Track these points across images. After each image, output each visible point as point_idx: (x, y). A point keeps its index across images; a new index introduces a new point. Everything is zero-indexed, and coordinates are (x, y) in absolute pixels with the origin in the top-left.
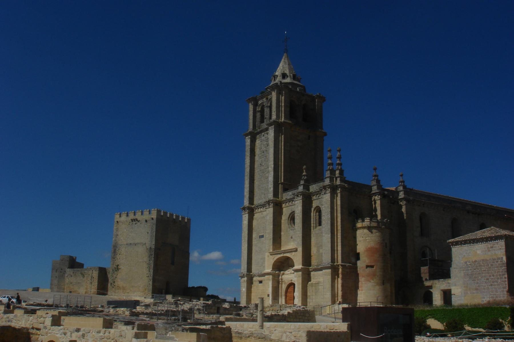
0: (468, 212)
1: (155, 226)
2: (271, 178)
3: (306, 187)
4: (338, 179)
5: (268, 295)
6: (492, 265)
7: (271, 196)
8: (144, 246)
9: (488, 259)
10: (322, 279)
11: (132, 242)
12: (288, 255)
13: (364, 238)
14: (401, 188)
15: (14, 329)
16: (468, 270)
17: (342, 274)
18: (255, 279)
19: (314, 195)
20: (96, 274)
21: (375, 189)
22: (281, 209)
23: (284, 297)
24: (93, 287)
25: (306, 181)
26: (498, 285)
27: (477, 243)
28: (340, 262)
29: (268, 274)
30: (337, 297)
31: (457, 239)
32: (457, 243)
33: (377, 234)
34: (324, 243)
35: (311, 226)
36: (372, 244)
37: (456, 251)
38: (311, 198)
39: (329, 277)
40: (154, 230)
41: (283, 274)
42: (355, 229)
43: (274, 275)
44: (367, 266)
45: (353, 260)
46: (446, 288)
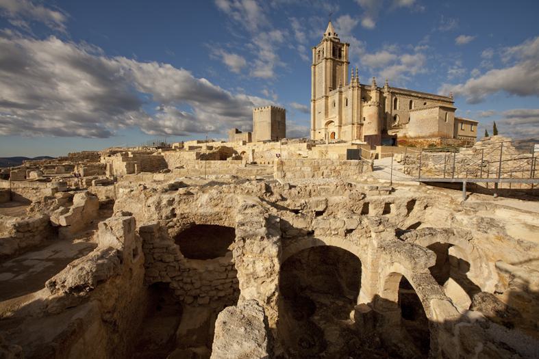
2: (324, 86)
7: (324, 94)
15: (228, 148)
34: (348, 113)
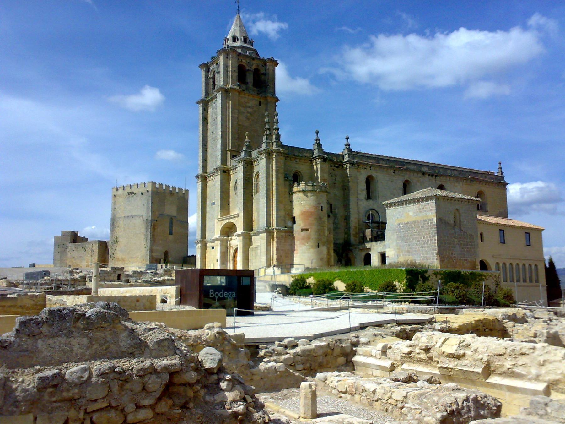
0: (424, 174)
1: (150, 199)
2: (219, 146)
3: (249, 153)
4: (275, 144)
5: (217, 261)
6: (423, 227)
7: (219, 164)
8: (141, 218)
9: (419, 220)
10: (259, 241)
11: (130, 215)
12: (231, 220)
13: (300, 202)
14: (346, 151)
16: (401, 232)
17: (277, 238)
18: (208, 245)
19: (255, 161)
20: (96, 248)
21: (316, 153)
22: (229, 175)
23: (232, 262)
24: (93, 260)
25: (248, 147)
26: (428, 247)
27: (410, 203)
28: (275, 226)
29: (217, 240)
30: (273, 260)
31: (391, 201)
32: (391, 205)
33: (313, 197)
35: (253, 192)
36: (307, 208)
37: (390, 212)
38: (252, 164)
39: (264, 241)
40: (150, 202)
41: (231, 239)
42: (291, 193)
43: (222, 241)
44: (302, 230)
45: (289, 224)
46: (383, 251)
